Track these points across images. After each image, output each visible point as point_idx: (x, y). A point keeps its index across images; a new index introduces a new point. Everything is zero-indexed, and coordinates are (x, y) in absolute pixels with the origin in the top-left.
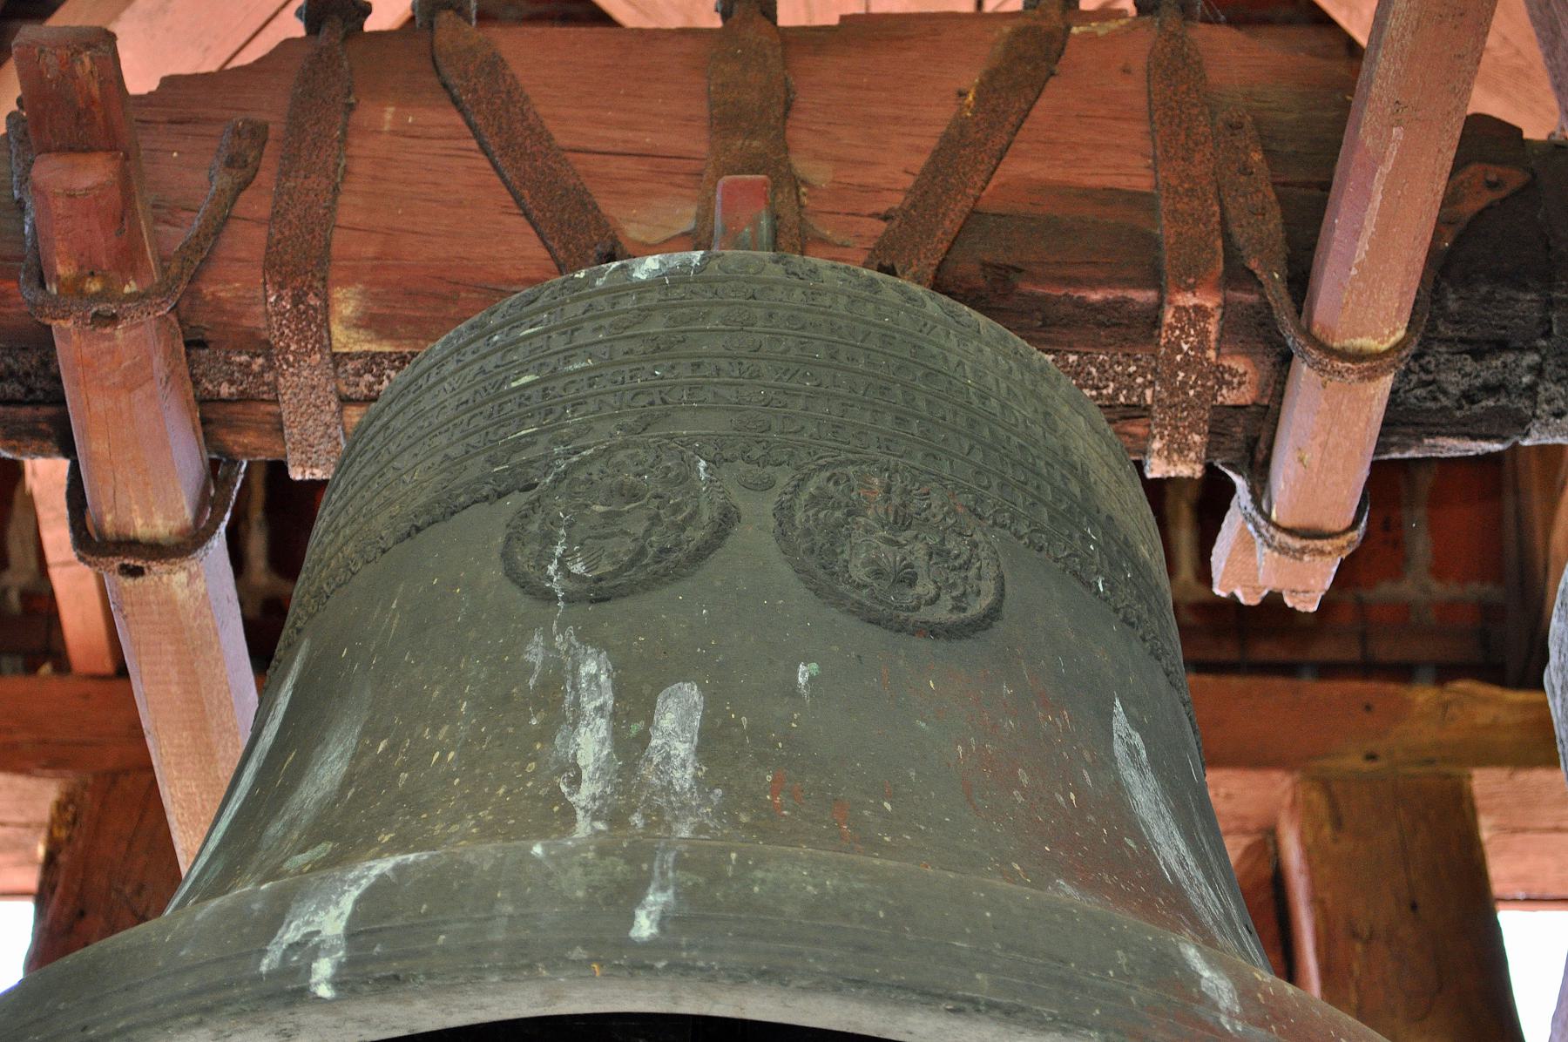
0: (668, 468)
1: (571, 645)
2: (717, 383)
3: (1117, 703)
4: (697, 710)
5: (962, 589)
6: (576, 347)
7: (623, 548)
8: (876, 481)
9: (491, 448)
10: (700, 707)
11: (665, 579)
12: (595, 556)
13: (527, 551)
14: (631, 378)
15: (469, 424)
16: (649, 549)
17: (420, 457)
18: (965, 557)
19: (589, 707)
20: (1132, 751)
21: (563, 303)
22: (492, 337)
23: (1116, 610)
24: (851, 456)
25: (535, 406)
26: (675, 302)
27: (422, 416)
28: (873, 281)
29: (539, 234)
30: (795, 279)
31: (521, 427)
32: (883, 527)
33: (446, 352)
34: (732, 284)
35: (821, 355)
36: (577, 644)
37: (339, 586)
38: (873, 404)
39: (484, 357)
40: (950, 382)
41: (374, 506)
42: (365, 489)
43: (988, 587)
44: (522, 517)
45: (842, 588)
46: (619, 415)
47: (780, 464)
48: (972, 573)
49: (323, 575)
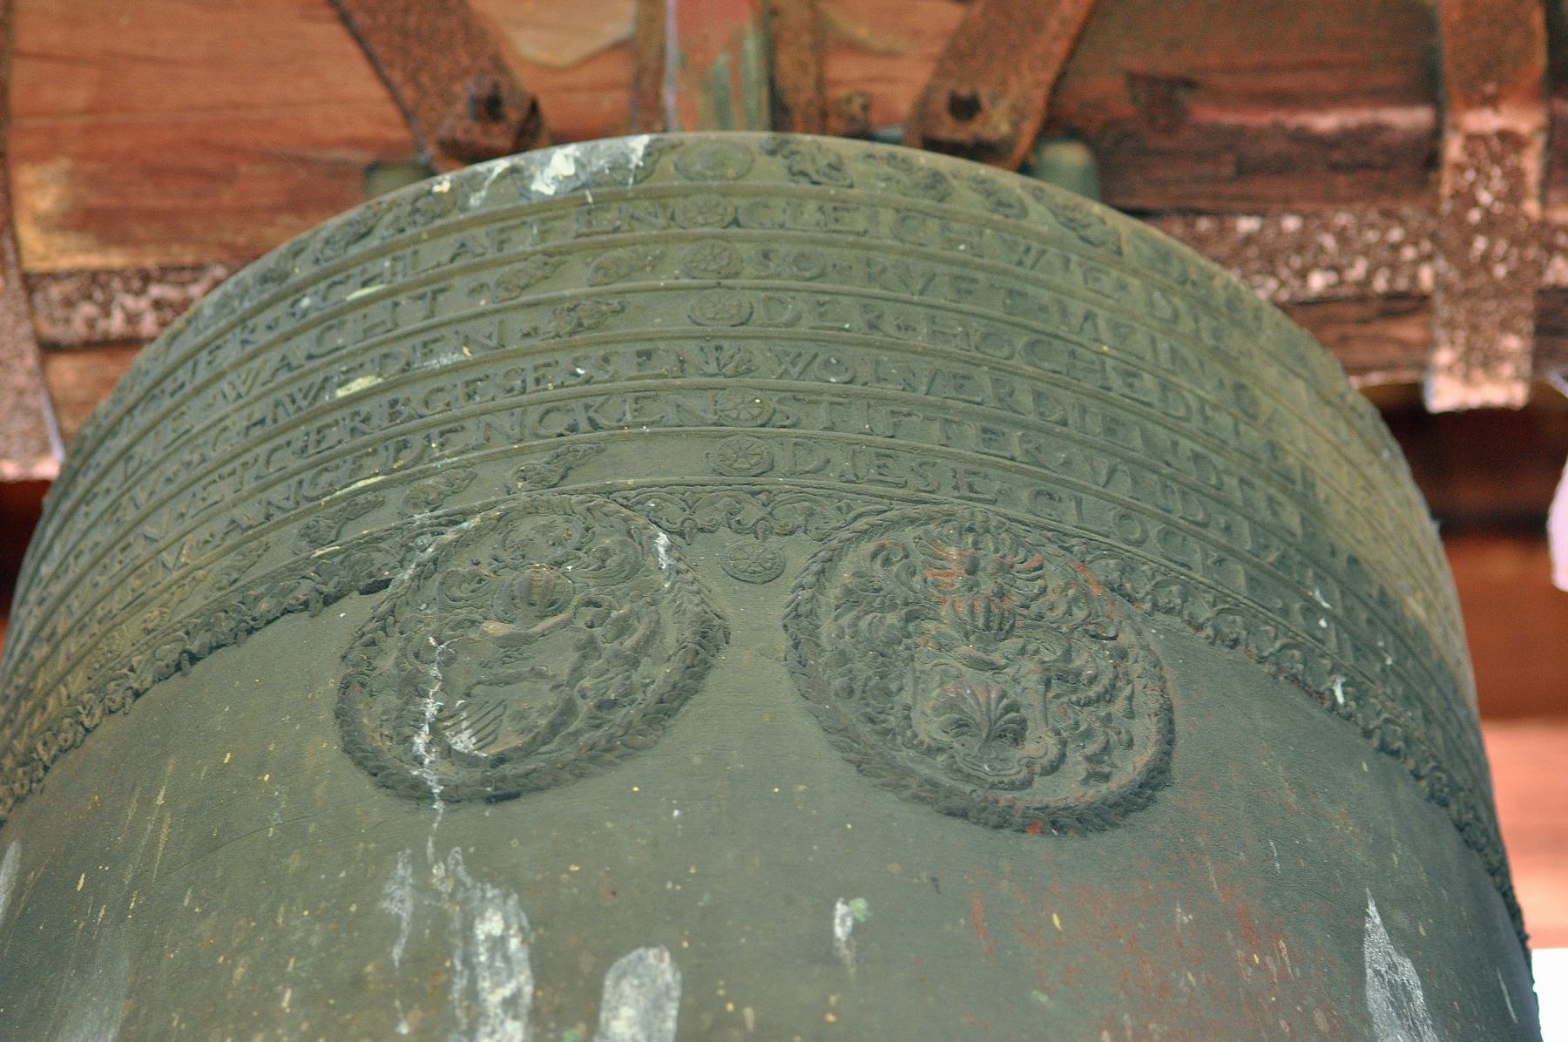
0: (606, 551)
1: (459, 883)
2: (682, 388)
3: (1372, 909)
4: (670, 999)
5: (1102, 738)
6: (442, 325)
7: (539, 703)
8: (953, 552)
9: (307, 513)
10: (676, 993)
11: (608, 756)
12: (491, 716)
13: (378, 708)
14: (538, 381)
15: (268, 462)
16: (579, 701)
17: (188, 523)
18: (1105, 681)
19: (494, 998)
20: (1400, 996)
21: (416, 240)
22: (297, 301)
23: (1367, 734)
24: (910, 510)
25: (378, 434)
26: (604, 238)
27: (188, 441)
28: (936, 178)
29: (370, 57)
30: (805, 185)
31: (354, 475)
32: (967, 635)
33: (222, 323)
34: (699, 199)
35: (854, 322)
36: (469, 881)
37: (64, 750)
38: (943, 408)
39: (287, 338)
40: (1073, 354)
41: (115, 604)
42: (98, 568)
43: (1146, 729)
44: (366, 645)
45: (904, 756)
46: (520, 452)
47: (792, 533)
48: (1118, 707)
49: (36, 724)
